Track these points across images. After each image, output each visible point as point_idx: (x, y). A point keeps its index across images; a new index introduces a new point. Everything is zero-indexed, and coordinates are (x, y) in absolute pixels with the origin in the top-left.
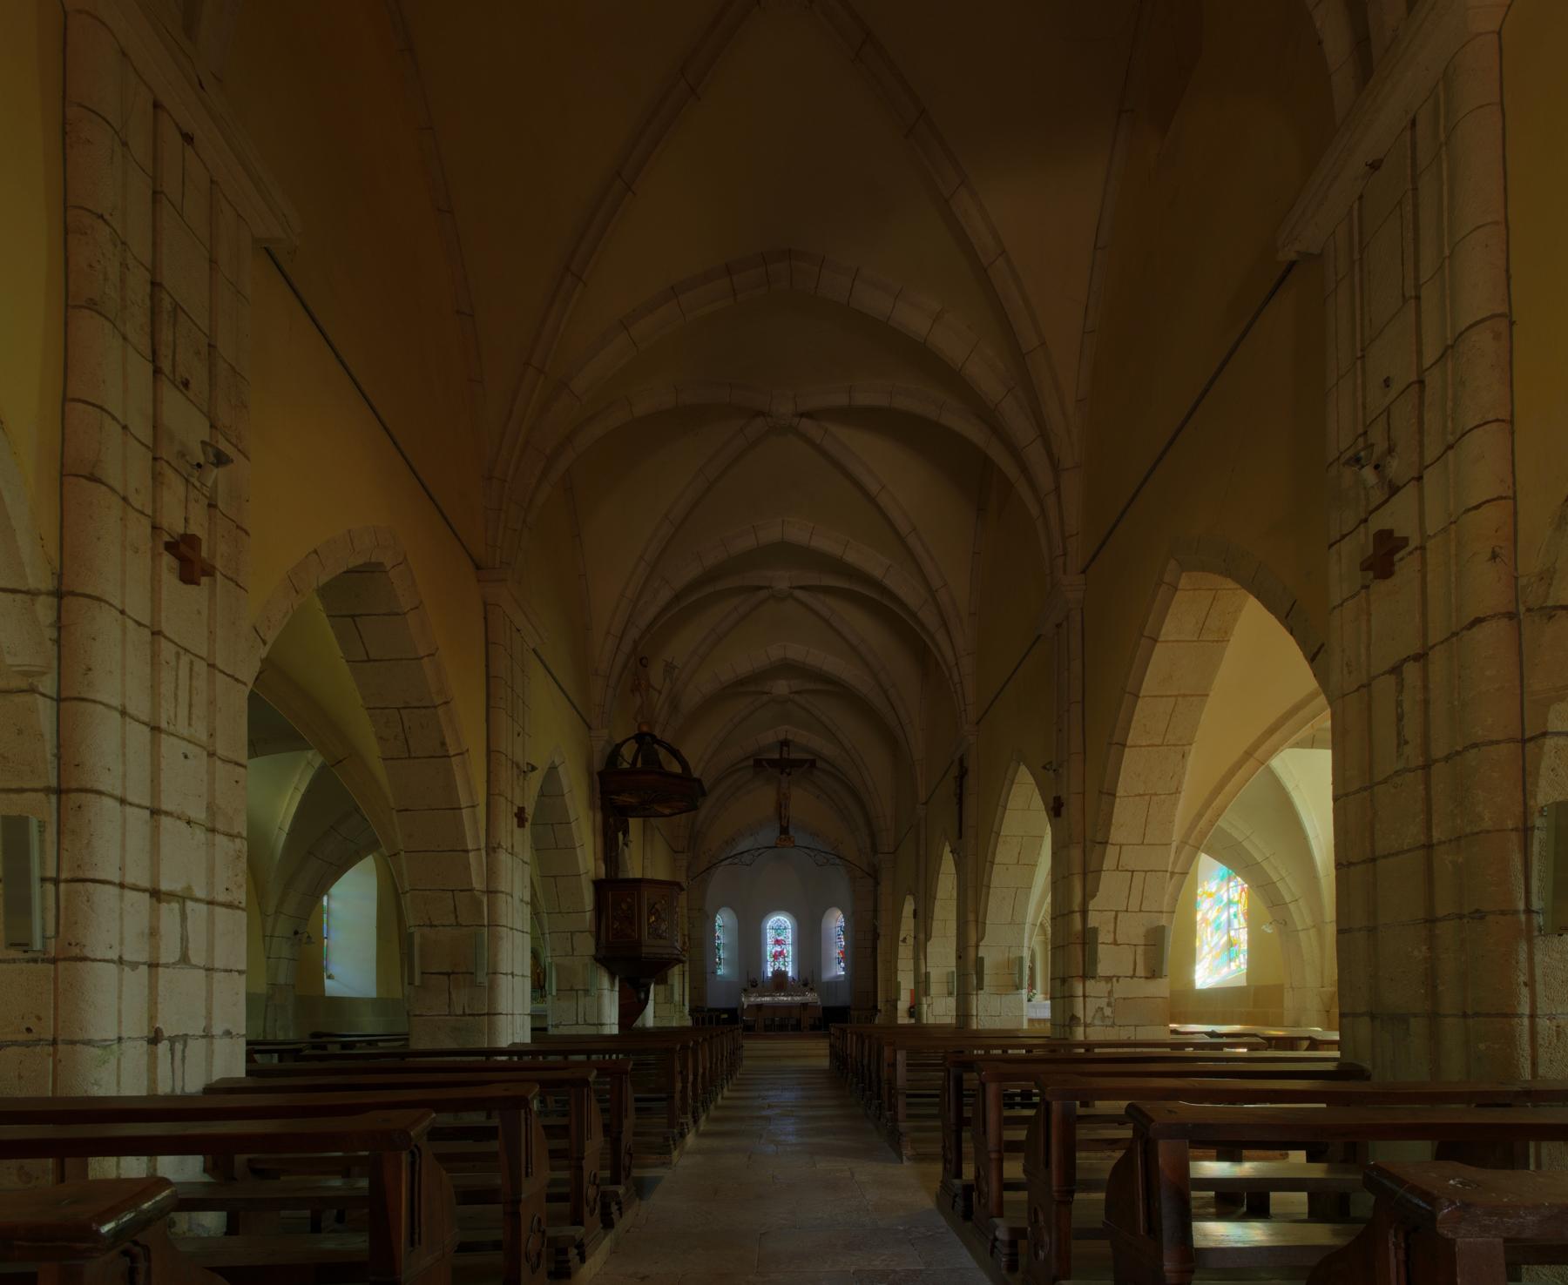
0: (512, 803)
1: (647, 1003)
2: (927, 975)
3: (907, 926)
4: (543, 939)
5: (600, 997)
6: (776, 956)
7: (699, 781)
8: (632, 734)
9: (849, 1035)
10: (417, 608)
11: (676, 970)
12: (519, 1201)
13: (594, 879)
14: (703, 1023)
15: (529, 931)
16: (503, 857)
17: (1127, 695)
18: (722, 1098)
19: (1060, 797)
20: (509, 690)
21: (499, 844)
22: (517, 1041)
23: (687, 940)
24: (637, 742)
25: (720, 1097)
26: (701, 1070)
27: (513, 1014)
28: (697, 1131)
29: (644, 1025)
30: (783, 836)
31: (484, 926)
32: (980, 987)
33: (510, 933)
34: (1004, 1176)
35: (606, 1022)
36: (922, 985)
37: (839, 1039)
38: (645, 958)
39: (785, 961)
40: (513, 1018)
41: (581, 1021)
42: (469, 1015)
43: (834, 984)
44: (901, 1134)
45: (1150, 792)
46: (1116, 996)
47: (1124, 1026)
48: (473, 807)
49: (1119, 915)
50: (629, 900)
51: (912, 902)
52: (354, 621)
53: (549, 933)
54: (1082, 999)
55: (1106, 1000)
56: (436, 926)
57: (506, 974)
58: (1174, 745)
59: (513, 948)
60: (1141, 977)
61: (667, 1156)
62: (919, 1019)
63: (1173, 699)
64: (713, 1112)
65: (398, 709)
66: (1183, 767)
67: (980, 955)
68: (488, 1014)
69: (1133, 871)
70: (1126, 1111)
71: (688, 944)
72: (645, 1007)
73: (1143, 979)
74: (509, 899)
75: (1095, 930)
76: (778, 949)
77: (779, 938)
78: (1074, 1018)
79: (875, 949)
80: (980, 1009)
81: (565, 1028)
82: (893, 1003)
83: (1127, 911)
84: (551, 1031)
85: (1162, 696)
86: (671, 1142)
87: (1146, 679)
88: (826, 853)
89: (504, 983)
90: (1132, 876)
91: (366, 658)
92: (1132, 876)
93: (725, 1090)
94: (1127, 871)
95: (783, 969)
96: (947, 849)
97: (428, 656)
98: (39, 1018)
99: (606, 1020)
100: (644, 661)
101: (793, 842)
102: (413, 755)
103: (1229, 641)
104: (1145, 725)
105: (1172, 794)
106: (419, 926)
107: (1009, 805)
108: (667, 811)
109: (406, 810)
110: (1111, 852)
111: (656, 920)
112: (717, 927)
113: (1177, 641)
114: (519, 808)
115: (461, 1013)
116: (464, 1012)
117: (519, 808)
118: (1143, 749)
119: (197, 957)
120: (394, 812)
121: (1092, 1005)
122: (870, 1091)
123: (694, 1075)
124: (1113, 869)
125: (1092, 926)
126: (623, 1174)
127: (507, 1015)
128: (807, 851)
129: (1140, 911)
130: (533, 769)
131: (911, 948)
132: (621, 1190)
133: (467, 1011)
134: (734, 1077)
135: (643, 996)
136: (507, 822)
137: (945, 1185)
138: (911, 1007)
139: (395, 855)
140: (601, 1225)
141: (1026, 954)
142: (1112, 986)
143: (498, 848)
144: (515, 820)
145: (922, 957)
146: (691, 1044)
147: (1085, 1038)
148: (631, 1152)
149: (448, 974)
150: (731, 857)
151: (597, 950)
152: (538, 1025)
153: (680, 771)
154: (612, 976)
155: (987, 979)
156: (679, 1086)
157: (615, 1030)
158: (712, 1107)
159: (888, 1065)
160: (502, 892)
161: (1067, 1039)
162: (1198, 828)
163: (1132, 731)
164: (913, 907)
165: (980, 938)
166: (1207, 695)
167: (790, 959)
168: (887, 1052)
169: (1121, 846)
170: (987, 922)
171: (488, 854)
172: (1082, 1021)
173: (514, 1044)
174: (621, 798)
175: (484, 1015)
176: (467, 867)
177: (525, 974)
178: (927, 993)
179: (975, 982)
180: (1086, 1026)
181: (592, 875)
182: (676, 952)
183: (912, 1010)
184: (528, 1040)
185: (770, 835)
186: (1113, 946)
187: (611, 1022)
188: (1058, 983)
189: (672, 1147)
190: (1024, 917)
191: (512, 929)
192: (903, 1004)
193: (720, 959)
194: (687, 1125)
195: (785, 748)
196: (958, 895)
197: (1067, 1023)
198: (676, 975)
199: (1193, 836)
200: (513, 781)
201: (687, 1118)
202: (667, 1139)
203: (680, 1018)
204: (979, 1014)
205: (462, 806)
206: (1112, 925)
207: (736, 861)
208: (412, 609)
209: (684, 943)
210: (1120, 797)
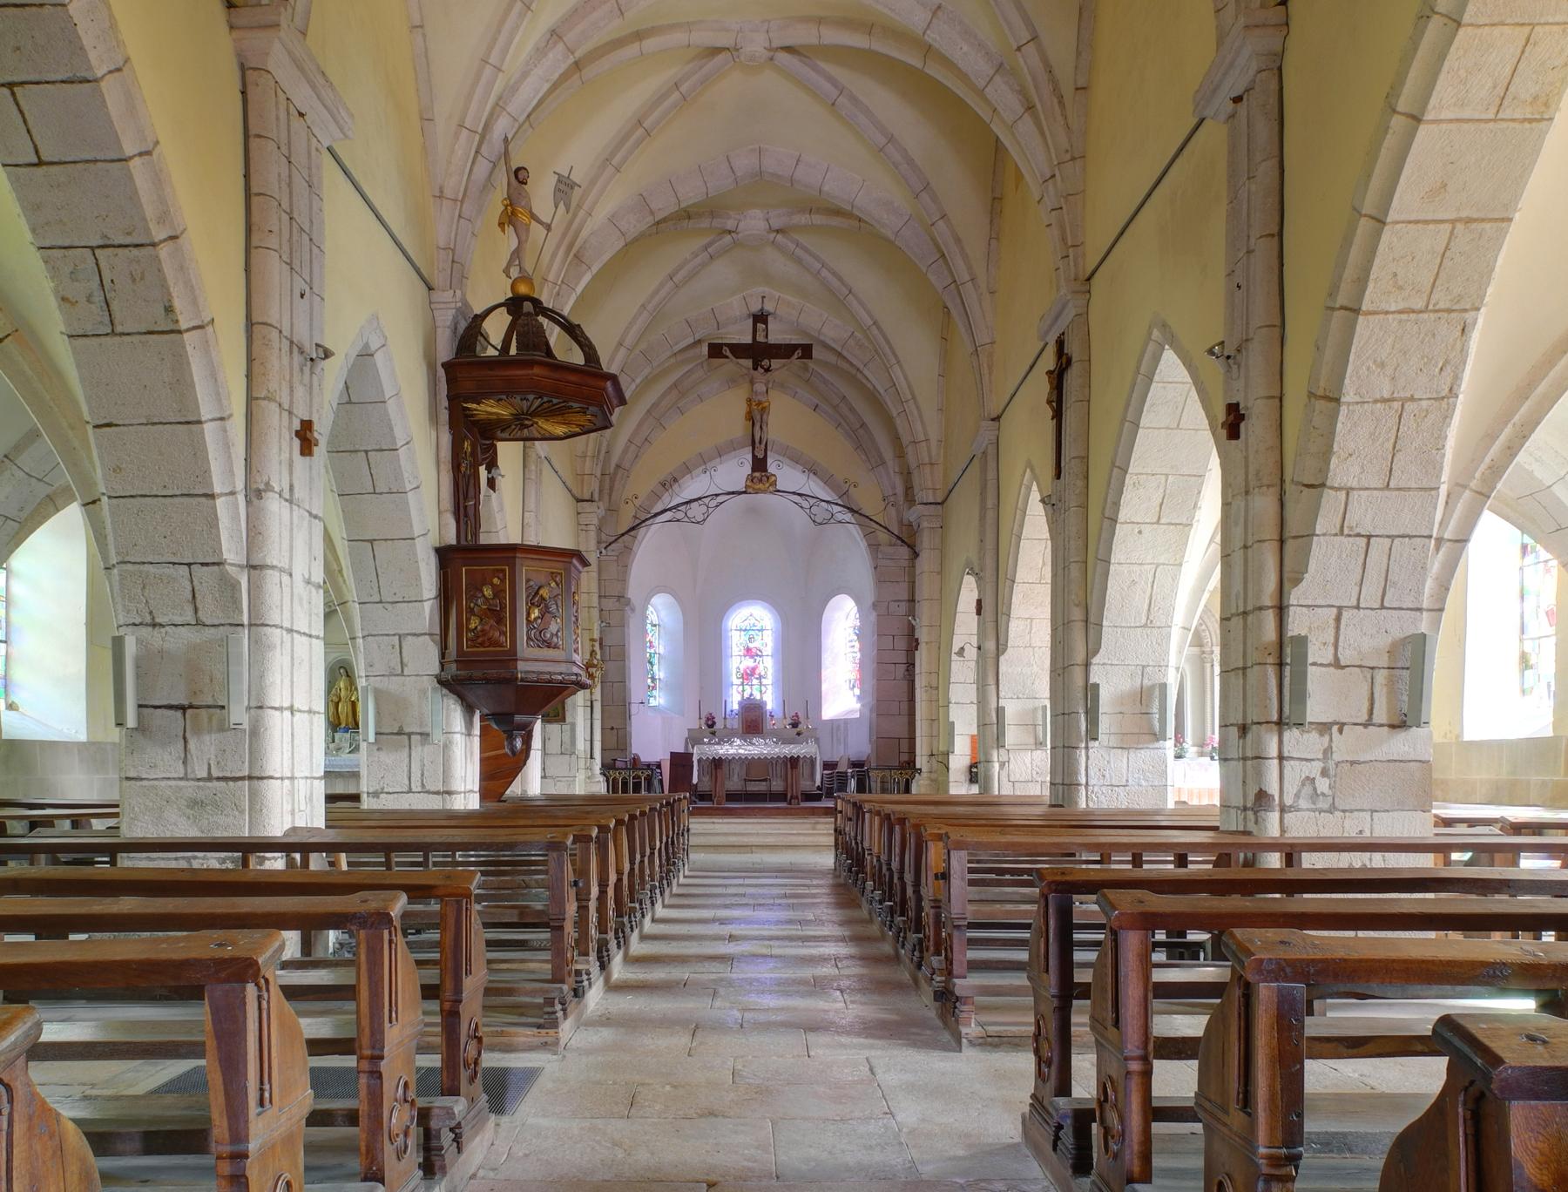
0: (290, 413)
1: (527, 756)
2: (1000, 712)
3: (966, 626)
4: (354, 647)
5: (447, 747)
6: (748, 675)
7: (613, 378)
8: (502, 300)
9: (867, 815)
10: (119, 70)
11: (580, 698)
12: (244, 1156)
13: (438, 545)
14: (625, 790)
15: (322, 635)
16: (274, 506)
17: (1363, 221)
18: (653, 920)
19: (1237, 405)
20: (285, 217)
21: (267, 484)
22: (300, 823)
23: (597, 648)
24: (509, 312)
25: (648, 919)
26: (613, 878)
27: (292, 778)
28: (607, 980)
29: (525, 791)
30: (757, 474)
31: (242, 625)
32: (1092, 735)
33: (287, 637)
34: (1154, 1094)
35: (454, 788)
36: (991, 730)
37: (850, 819)
38: (522, 680)
39: (761, 684)
40: (293, 785)
41: (416, 786)
42: (218, 779)
43: (837, 726)
44: (958, 999)
45: (1402, 395)
46: (1337, 757)
47: (1351, 811)
48: (222, 419)
49: (1345, 614)
50: (496, 581)
51: (974, 585)
52: (13, 94)
53: (363, 637)
54: (1276, 762)
55: (1321, 764)
56: (161, 625)
57: (280, 709)
58: (1449, 311)
59: (293, 665)
60: (1381, 725)
61: (551, 1031)
62: (986, 788)
63: (1448, 227)
64: (636, 947)
65: (92, 248)
66: (1462, 350)
67: (1092, 680)
68: (250, 778)
69: (1369, 537)
70: (1434, 1030)
71: (598, 657)
72: (525, 764)
73: (1386, 728)
74: (286, 578)
75: (1301, 642)
76: (749, 663)
77: (751, 645)
78: (1262, 796)
79: (911, 665)
80: (1091, 773)
81: (390, 797)
82: (942, 759)
83: (1358, 607)
84: (367, 803)
85: (1426, 222)
86: (558, 1007)
87: (1399, 190)
88: (828, 502)
89: (277, 726)
90: (1368, 544)
91: (35, 160)
92: (1368, 544)
93: (658, 906)
94: (1358, 535)
95: (758, 697)
96: (1035, 496)
97: (140, 154)
99: (458, 785)
100: (521, 175)
101: (775, 483)
102: (119, 329)
103: (1551, 119)
104: (1395, 275)
105: (1443, 398)
106: (135, 625)
107: (1144, 422)
108: (560, 430)
110: (1331, 503)
111: (542, 617)
112: (649, 627)
113: (1458, 120)
114: (303, 422)
115: (205, 775)
116: (209, 773)
117: (303, 422)
118: (1390, 317)
120: (89, 428)
121: (1294, 771)
122: (902, 915)
123: (600, 885)
124: (1333, 532)
125: (1295, 633)
126: (464, 1075)
127: (282, 779)
128: (797, 498)
129: (1383, 607)
130: (327, 354)
131: (973, 665)
132: (459, 1106)
133: (215, 773)
134: (674, 882)
135: (519, 743)
136: (280, 446)
137: (1037, 1101)
138: (973, 765)
139: (94, 502)
140: (421, 1173)
141: (1172, 680)
142: (1331, 740)
143: (265, 491)
144: (297, 443)
145: (991, 680)
146: (595, 832)
147: (1283, 831)
148: (479, 1034)
149: (183, 708)
150: (670, 509)
151: (442, 665)
152: (340, 788)
153: (582, 362)
154: (469, 709)
155: (1104, 724)
156: (571, 908)
157: (474, 803)
158: (634, 938)
159: (936, 875)
160: (273, 567)
161: (1248, 833)
162: (1487, 460)
163: (1371, 285)
164: (975, 596)
165: (1093, 649)
166: (1510, 220)
167: (768, 681)
168: (934, 853)
169: (1348, 491)
170: (1105, 623)
171: (248, 502)
172: (1277, 802)
173: (294, 829)
174: (482, 407)
175: (242, 778)
176: (213, 523)
177: (315, 708)
178: (1000, 742)
179: (1083, 728)
180: (1283, 810)
181: (434, 540)
182: (575, 670)
183: (974, 770)
184: (320, 823)
185: (735, 471)
186: (1332, 669)
187: (466, 794)
188: (1234, 732)
189: (560, 1014)
190: (1169, 613)
191: (290, 631)
192: (960, 759)
193: (653, 679)
194: (588, 973)
195: (761, 326)
196: (1054, 575)
197: (1249, 805)
198: (578, 705)
199: (1478, 475)
200: (292, 375)
201: (588, 962)
202: (550, 1002)
203: (586, 781)
204: (1091, 782)
205: (203, 419)
206: (1331, 632)
207: (680, 515)
208: (110, 72)
209: (593, 653)
210: (1349, 404)
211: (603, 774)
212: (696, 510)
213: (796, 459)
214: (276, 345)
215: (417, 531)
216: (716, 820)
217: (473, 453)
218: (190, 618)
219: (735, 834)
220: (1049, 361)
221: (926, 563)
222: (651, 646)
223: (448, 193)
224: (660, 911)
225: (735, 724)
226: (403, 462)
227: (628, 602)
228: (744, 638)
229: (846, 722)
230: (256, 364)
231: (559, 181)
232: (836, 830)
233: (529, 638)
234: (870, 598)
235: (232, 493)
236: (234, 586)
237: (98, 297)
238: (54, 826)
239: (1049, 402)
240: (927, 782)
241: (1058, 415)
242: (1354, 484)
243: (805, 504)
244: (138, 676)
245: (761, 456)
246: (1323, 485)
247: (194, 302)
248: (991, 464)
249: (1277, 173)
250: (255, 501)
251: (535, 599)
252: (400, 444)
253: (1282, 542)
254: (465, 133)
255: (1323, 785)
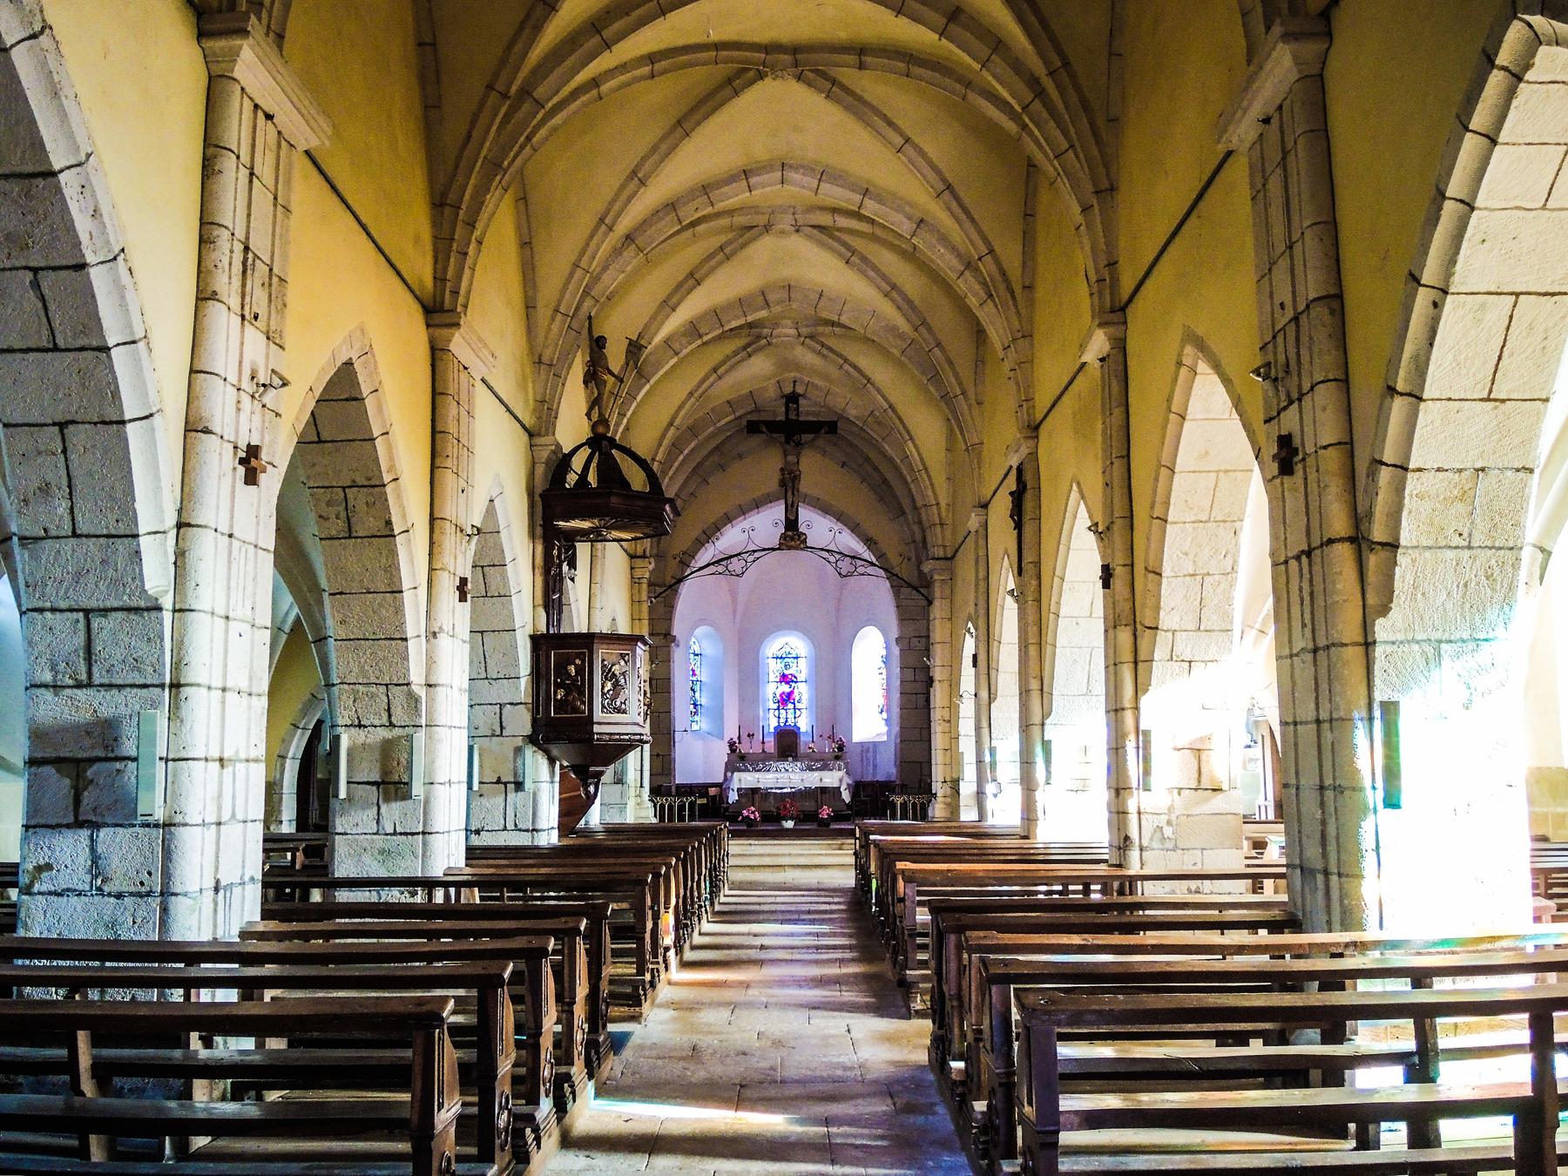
18: (700, 934)
33: (449, 731)
41: (510, 826)
42: (401, 834)
43: (869, 749)
56: (365, 727)
76: (785, 688)
77: (786, 672)
89: (441, 793)
91: (316, 439)
98: (150, 874)
99: (542, 824)
101: (805, 541)
102: (354, 534)
109: (341, 593)
110: (1163, 639)
119: (240, 816)
128: (825, 554)
133: (398, 830)
135: (592, 789)
154: (552, 761)
165: (1046, 715)
172: (1137, 843)
175: (418, 834)
181: (529, 630)
202: (636, 989)
205: (57, 167)
211: (651, 800)
212: (736, 565)
213: (825, 509)
214: (448, 531)
215: (518, 624)
216: (752, 842)
217: (559, 557)
218: (385, 721)
219: (769, 855)
220: (1011, 484)
221: (938, 610)
222: (694, 674)
223: (545, 359)
224: (707, 927)
225: (771, 746)
226: (509, 574)
227: (674, 639)
228: (780, 665)
229: (875, 744)
230: (435, 546)
231: (630, 344)
232: (855, 854)
233: (603, 706)
234: (894, 633)
235: (418, 636)
236: (417, 700)
237: (343, 515)
238: (1343, 989)
239: (1012, 517)
240: (942, 806)
241: (1019, 526)
242: (1177, 628)
243: (832, 559)
244: (349, 762)
245: (792, 518)
246: (1157, 628)
247: (404, 516)
248: (982, 542)
249: (1124, 415)
250: (433, 640)
251: (609, 675)
252: (507, 561)
253: (1136, 663)
254: (559, 317)
255: (1168, 831)
